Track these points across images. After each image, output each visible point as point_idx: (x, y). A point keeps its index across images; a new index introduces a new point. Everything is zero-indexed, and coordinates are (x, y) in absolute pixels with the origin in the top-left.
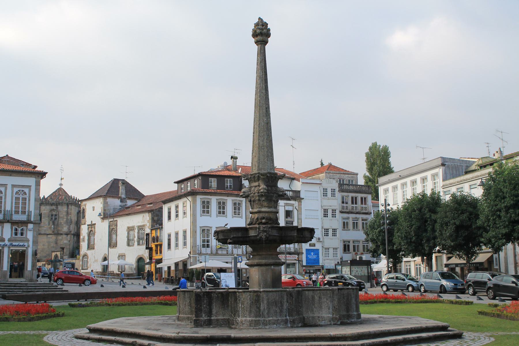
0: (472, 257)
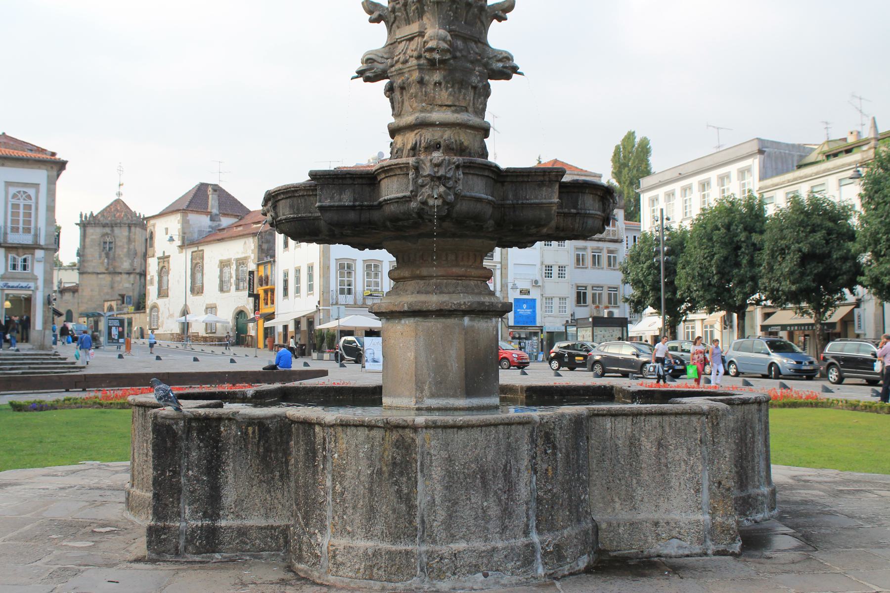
0: (824, 312)
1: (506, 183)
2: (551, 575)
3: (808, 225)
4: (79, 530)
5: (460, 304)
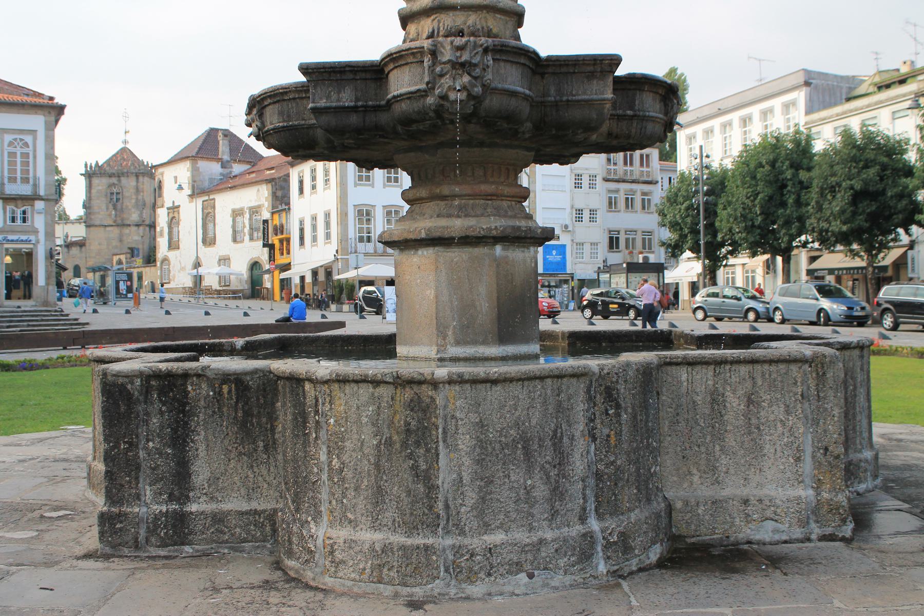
0: (876, 255)
1: (546, 76)
2: (615, 572)
3: (861, 161)
4: (25, 515)
5: (490, 229)
